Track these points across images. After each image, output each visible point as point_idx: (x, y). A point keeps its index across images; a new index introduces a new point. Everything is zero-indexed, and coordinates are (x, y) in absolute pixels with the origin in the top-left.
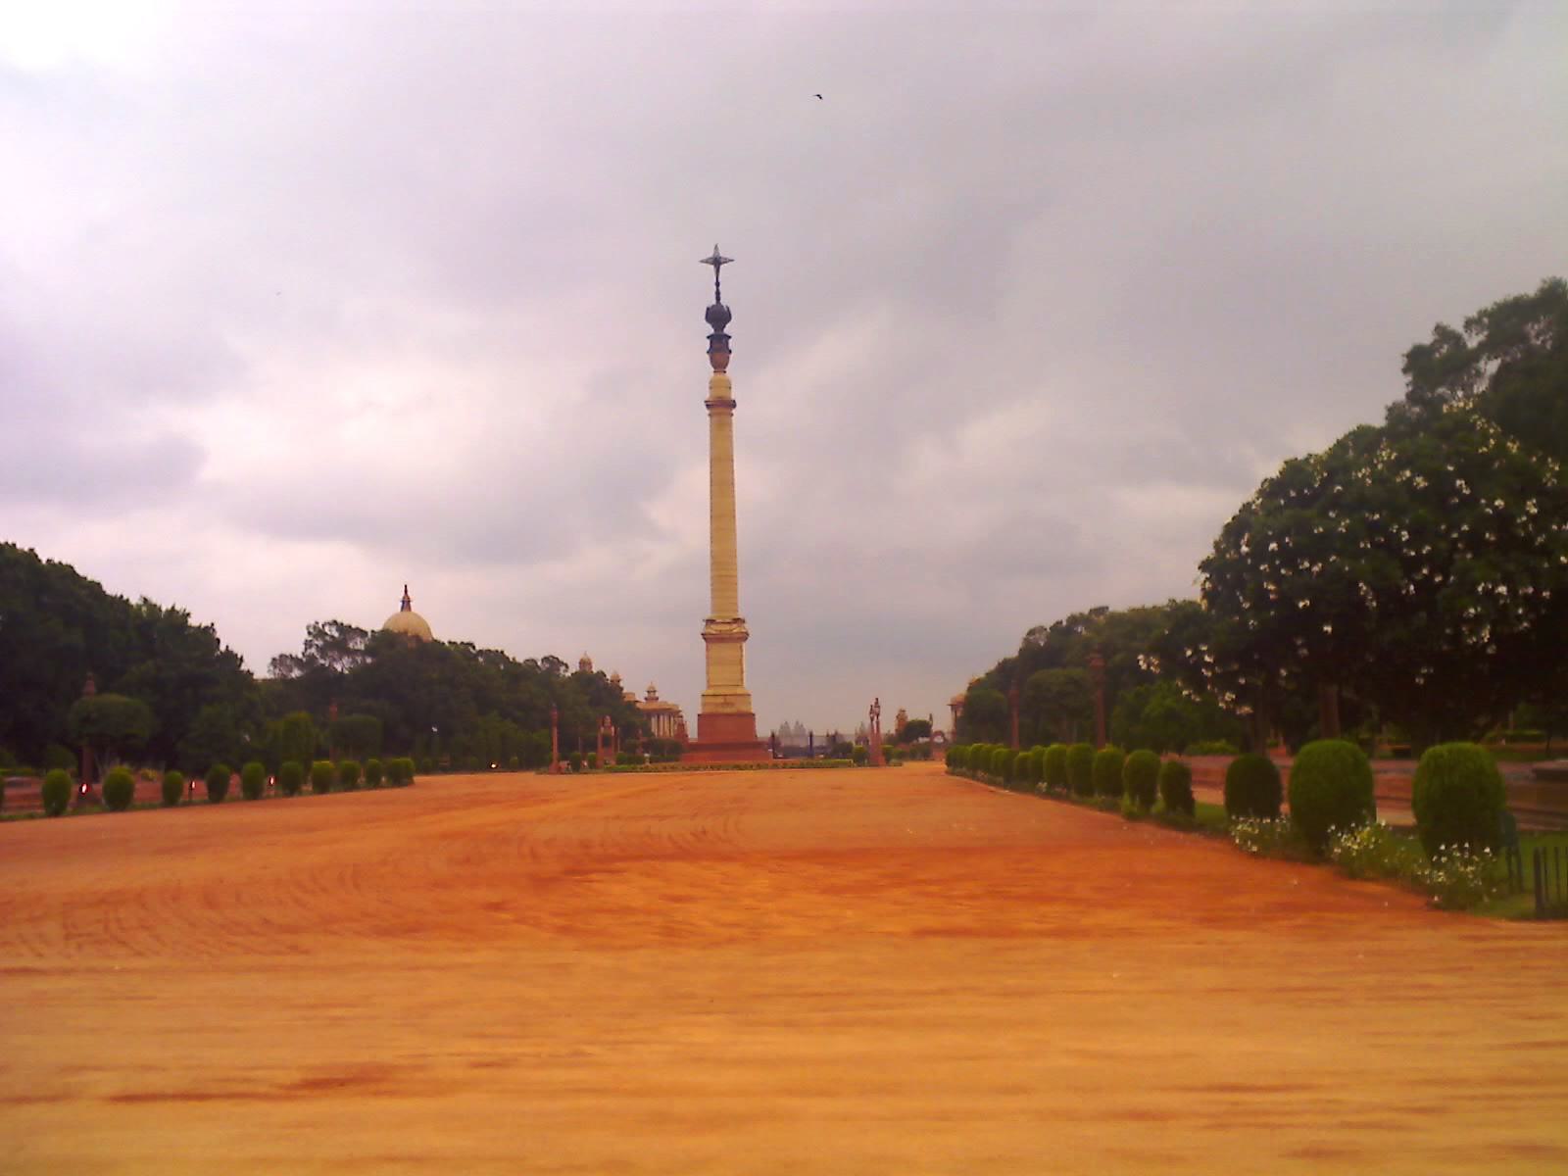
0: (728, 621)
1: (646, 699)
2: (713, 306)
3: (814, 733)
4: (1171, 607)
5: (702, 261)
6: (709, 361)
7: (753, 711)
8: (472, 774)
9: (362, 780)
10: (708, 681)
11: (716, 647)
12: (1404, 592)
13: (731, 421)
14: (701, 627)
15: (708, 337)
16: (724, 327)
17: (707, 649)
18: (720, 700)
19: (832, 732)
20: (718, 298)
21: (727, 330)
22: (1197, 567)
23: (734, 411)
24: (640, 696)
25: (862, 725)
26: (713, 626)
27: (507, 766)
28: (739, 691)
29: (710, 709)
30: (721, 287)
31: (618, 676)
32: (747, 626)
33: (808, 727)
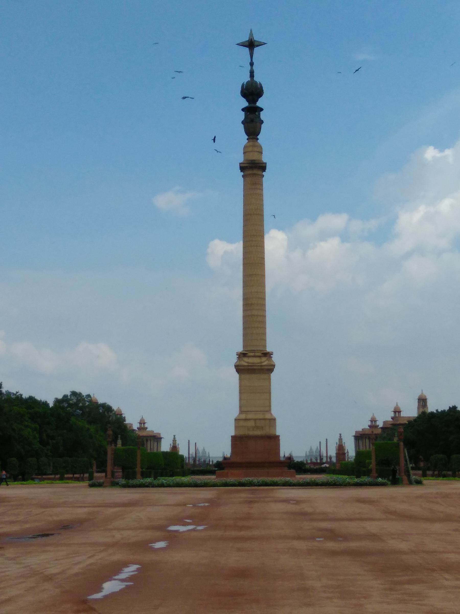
0: (259, 354)
1: (138, 428)
5: (238, 44)
7: (277, 434)
10: (240, 407)
11: (246, 376)
12: (201, 461)
13: (263, 179)
14: (234, 359)
15: (243, 110)
17: (240, 379)
21: (260, 103)
23: (264, 173)
25: (311, 449)
26: (246, 359)
28: (268, 416)
29: (242, 432)
30: (254, 67)
31: (144, 420)
32: (275, 359)
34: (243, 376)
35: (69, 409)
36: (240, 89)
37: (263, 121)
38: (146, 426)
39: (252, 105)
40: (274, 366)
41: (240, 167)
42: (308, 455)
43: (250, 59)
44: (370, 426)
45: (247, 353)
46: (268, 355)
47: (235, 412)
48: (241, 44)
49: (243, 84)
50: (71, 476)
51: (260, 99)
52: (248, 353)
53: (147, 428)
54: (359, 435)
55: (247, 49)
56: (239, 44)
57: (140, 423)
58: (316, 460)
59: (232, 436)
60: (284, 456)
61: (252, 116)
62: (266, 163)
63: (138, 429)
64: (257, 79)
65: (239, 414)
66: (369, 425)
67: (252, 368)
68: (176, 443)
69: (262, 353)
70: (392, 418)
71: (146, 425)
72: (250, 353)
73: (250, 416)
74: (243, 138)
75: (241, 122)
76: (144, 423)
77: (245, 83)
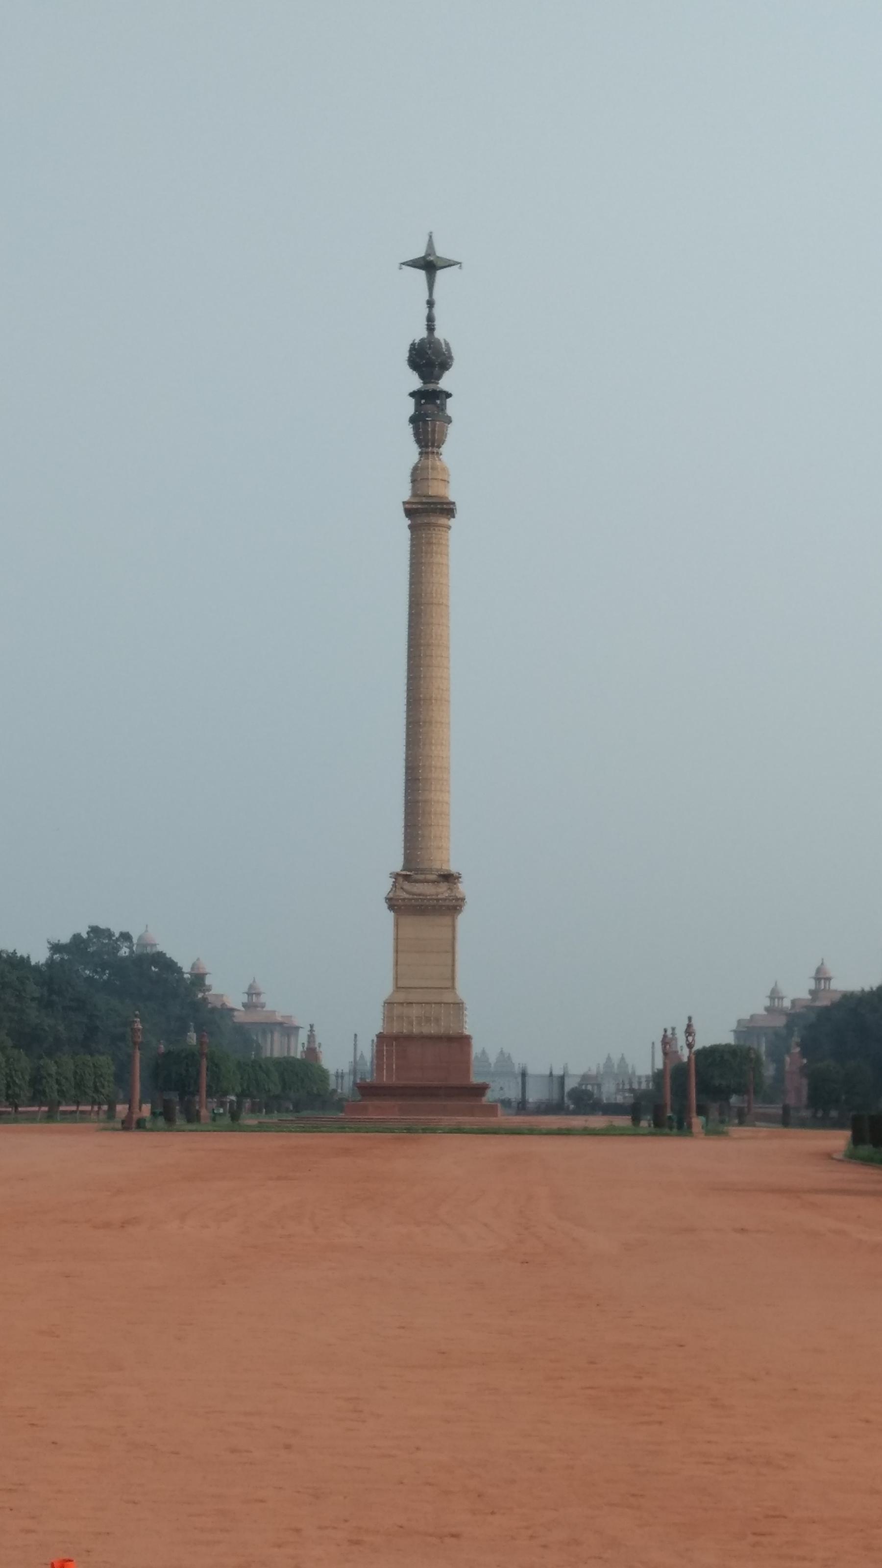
1: (244, 1005)
2: (422, 340)
3: (530, 1071)
4: (8, 956)
6: (412, 438)
7: (467, 1032)
8: (32, 1123)
10: (396, 979)
14: (386, 885)
15: (413, 395)
16: (439, 377)
17: (397, 925)
19: (558, 1071)
20: (431, 328)
21: (445, 383)
24: (235, 1000)
25: (609, 1058)
27: (67, 1111)
28: (447, 997)
32: (464, 888)
33: (519, 1060)
35: (104, 941)
39: (431, 387)
40: (463, 899)
42: (602, 1073)
44: (767, 1009)
46: (449, 878)
47: (386, 989)
48: (411, 263)
49: (413, 345)
50: (74, 1108)
52: (412, 875)
54: (744, 1030)
55: (421, 274)
56: (408, 263)
58: (640, 1083)
61: (430, 408)
62: (454, 503)
63: (243, 1006)
64: (440, 334)
65: (393, 993)
68: (314, 1042)
69: (440, 876)
70: (812, 992)
71: (263, 999)
73: (414, 997)
74: (411, 453)
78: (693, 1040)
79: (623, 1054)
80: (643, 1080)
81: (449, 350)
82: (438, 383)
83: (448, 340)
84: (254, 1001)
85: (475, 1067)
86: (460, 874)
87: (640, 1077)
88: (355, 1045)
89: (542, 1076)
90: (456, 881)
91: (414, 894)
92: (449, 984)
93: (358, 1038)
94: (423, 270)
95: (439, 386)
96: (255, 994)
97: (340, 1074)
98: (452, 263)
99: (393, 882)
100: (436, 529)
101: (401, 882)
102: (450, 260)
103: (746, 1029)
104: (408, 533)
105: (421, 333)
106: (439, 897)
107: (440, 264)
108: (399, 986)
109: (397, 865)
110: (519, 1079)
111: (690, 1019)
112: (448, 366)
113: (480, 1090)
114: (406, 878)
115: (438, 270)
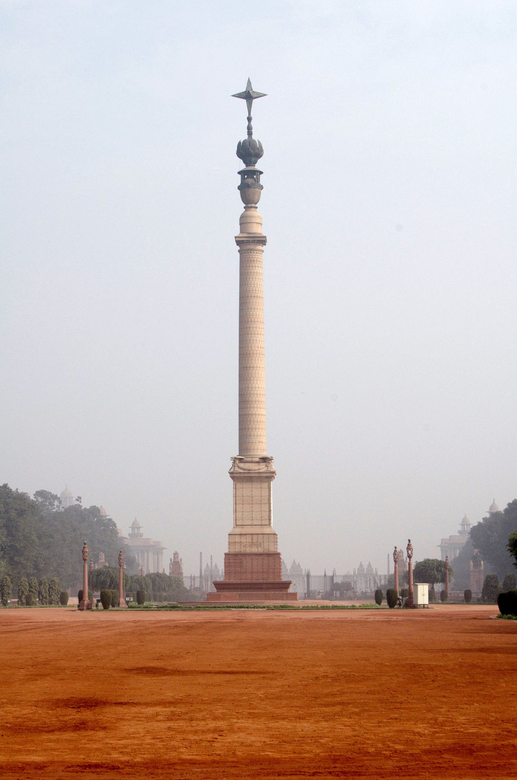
0: (257, 460)
1: (130, 535)
2: (244, 141)
3: (312, 574)
5: (233, 96)
7: (279, 551)
9: (398, 751)
15: (239, 173)
16: (255, 162)
18: (249, 539)
19: (329, 574)
20: (250, 133)
21: (259, 166)
22: (243, 207)
24: (14, 489)
25: (361, 565)
28: (267, 530)
29: (237, 549)
30: (252, 123)
32: (274, 466)
33: (304, 567)
34: (239, 485)
36: (236, 149)
37: (262, 186)
38: (141, 532)
39: (250, 168)
41: (236, 241)
43: (248, 113)
44: (459, 532)
45: (243, 459)
47: (230, 527)
48: (237, 95)
49: (240, 143)
51: (259, 161)
53: (141, 535)
55: (244, 101)
56: (235, 96)
57: (133, 528)
59: (226, 554)
60: (325, 575)
61: (250, 181)
62: (265, 237)
66: (459, 531)
67: (249, 475)
68: (178, 557)
69: (261, 458)
71: (142, 531)
72: (246, 458)
75: (237, 187)
76: (139, 528)
77: (242, 141)
78: (412, 553)
79: (513, 564)
80: (383, 578)
81: (261, 147)
82: (255, 166)
83: (260, 140)
84: (136, 532)
85: (283, 572)
86: (272, 457)
87: (380, 576)
88: (201, 559)
89: (320, 577)
90: (270, 461)
91: (244, 470)
92: (267, 523)
93: (203, 555)
94: (245, 99)
95: (255, 167)
96: (137, 528)
97: (193, 578)
98: (262, 95)
99: (233, 463)
100: (255, 252)
101: (237, 463)
102: (260, 93)
103: (445, 546)
104: (238, 255)
105: (245, 137)
106: (260, 471)
107: (254, 95)
108: (238, 523)
109: (236, 453)
110: (306, 579)
111: (409, 541)
112: (261, 155)
113: (286, 585)
114: (241, 460)
115: (254, 99)
